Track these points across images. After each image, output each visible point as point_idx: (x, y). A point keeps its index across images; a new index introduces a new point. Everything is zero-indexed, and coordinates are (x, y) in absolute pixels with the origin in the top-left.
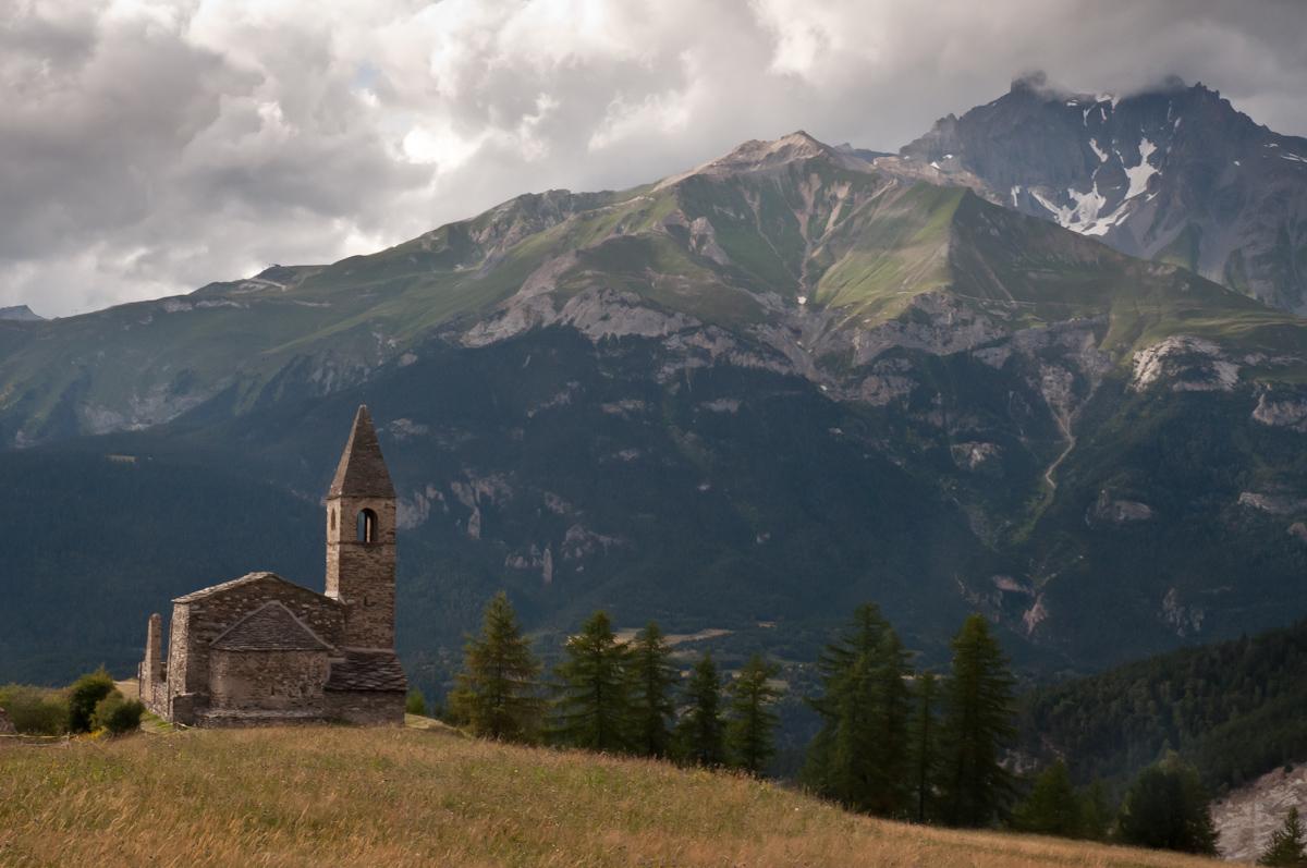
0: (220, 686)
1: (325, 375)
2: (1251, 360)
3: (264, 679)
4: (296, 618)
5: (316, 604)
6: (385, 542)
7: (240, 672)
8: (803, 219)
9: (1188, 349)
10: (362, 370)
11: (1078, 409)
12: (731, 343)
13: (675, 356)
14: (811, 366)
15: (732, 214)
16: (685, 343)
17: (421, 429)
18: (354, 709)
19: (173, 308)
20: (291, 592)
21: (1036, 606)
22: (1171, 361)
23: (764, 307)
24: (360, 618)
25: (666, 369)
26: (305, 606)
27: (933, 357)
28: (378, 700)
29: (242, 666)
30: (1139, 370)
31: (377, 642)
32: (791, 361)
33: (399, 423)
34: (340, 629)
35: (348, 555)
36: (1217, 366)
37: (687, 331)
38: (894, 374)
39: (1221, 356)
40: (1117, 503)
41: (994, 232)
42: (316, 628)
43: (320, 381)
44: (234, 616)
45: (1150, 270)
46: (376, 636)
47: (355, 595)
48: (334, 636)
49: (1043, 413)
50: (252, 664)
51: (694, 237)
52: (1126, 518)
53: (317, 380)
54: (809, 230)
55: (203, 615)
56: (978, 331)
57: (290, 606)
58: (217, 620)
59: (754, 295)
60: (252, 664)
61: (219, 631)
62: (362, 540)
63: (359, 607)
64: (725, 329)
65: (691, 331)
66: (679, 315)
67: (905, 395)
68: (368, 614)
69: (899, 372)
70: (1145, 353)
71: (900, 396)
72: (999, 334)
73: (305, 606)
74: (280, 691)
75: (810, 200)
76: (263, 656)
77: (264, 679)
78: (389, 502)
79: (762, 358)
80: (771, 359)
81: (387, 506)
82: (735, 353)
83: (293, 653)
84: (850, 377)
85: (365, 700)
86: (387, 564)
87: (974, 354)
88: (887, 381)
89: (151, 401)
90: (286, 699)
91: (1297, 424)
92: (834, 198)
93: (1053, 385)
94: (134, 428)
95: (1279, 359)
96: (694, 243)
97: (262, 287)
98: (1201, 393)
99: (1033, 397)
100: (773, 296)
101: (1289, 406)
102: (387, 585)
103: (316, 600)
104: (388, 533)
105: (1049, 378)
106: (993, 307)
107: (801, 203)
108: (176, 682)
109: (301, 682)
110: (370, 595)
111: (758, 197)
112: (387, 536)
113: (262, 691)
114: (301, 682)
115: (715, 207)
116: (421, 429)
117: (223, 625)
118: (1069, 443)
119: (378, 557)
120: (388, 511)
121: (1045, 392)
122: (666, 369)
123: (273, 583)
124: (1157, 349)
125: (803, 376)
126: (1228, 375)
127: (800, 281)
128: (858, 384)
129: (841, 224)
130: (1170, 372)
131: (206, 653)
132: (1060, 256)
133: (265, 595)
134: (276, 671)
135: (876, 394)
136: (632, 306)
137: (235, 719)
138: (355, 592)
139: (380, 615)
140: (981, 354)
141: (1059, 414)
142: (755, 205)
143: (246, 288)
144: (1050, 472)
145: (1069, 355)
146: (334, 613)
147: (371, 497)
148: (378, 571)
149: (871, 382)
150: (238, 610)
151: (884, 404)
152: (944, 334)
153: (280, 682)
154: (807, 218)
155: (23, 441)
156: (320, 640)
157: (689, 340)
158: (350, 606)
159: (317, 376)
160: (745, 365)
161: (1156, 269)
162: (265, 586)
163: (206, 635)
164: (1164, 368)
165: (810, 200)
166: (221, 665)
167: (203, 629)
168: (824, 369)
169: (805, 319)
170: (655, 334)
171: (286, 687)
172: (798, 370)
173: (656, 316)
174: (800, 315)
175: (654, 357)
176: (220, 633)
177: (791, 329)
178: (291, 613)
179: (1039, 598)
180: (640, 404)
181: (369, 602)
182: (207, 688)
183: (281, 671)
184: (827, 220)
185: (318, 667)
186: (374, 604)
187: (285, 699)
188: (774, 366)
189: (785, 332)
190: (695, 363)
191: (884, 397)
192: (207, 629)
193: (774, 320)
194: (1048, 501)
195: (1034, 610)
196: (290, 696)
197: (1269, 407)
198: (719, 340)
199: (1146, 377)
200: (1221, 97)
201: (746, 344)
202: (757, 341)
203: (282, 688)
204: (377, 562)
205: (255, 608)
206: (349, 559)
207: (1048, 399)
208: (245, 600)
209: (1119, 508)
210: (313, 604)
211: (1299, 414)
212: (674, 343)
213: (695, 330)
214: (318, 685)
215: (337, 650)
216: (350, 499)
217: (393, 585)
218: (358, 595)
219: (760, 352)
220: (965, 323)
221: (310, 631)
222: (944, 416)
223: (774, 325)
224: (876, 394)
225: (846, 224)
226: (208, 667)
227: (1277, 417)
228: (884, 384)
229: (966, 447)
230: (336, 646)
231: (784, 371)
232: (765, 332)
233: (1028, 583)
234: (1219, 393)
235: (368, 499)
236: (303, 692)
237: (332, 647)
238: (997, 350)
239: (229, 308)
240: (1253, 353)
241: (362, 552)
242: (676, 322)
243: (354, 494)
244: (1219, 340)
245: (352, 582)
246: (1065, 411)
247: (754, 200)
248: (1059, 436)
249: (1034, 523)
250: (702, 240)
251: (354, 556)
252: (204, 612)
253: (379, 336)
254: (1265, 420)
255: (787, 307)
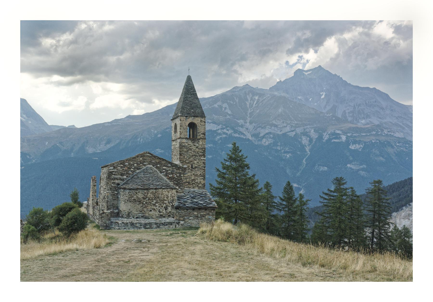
0: (123, 207)
1: (140, 139)
2: (349, 135)
3: (146, 203)
4: (159, 173)
5: (170, 167)
6: (201, 138)
7: (134, 199)
8: (248, 104)
9: (334, 132)
10: (149, 138)
11: (310, 146)
12: (233, 131)
13: (220, 134)
14: (250, 136)
15: (232, 103)
16: (222, 131)
17: (162, 151)
18: (190, 218)
19: (106, 125)
20: (157, 161)
21: (302, 190)
22: (331, 135)
23: (239, 123)
24: (189, 174)
25: (218, 137)
26: (164, 168)
27: (278, 134)
28: (202, 214)
29: (135, 196)
30: (324, 137)
31: (198, 186)
32: (246, 135)
33: (157, 150)
34: (181, 179)
35: (183, 144)
36: (341, 136)
37: (222, 129)
38: (269, 138)
39: (342, 134)
40: (319, 167)
41: (291, 106)
42: (169, 178)
43: (140, 141)
44: (130, 172)
45: (326, 115)
46: (197, 183)
47: (187, 163)
48: (178, 182)
49: (303, 147)
50: (140, 195)
51: (224, 108)
52: (322, 170)
53: (139, 141)
54: (249, 106)
55: (116, 172)
56: (288, 129)
57: (157, 168)
58: (122, 175)
59: (237, 121)
60: (140, 195)
61: (123, 180)
62: (188, 137)
63: (189, 169)
64: (231, 128)
65: (223, 129)
66: (221, 125)
67: (272, 143)
68: (193, 172)
69: (270, 138)
70: (325, 133)
71: (270, 143)
72: (293, 129)
73: (164, 168)
74: (154, 209)
75: (249, 99)
76: (145, 191)
77: (146, 203)
78: (203, 120)
79: (239, 135)
80: (241, 135)
81: (201, 121)
82: (233, 134)
83: (160, 190)
84: (259, 139)
85: (196, 213)
86: (202, 148)
87: (287, 133)
88: (267, 140)
89: (101, 146)
90: (157, 213)
91: (359, 149)
92: (255, 99)
93: (305, 141)
94: (98, 152)
95: (355, 134)
96: (224, 109)
97: (126, 120)
98: (338, 142)
99: (300, 143)
100: (242, 121)
101: (357, 145)
102: (202, 158)
103: (170, 165)
104: (202, 134)
105: (304, 139)
106: (291, 123)
107: (247, 100)
108: (102, 205)
109: (165, 205)
110: (194, 163)
111: (238, 99)
112: (202, 135)
113: (145, 209)
114: (165, 205)
115: (228, 101)
116: (162, 151)
117: (125, 177)
118: (308, 153)
119: (197, 145)
120: (202, 123)
121: (303, 142)
122: (218, 137)
123: (148, 156)
124: (328, 132)
125: (249, 138)
126: (344, 138)
127: (248, 117)
128: (261, 140)
129: (257, 105)
130: (331, 137)
131: (116, 191)
132: (305, 112)
133: (145, 162)
134: (152, 199)
135: (265, 143)
136: (210, 123)
137: (132, 224)
138: (187, 161)
139: (199, 173)
140: (289, 134)
141: (306, 147)
142: (237, 101)
143: (123, 120)
144: (304, 160)
145: (308, 134)
146: (178, 171)
147: (194, 116)
148: (198, 152)
149: (264, 140)
150: (132, 169)
151: (267, 145)
152: (280, 129)
153: (154, 205)
154: (249, 103)
155: (73, 155)
156: (171, 184)
157: (223, 130)
158: (185, 168)
159: (139, 139)
160: (236, 136)
161: (327, 115)
162: (145, 158)
163: (117, 181)
164: (330, 136)
165: (249, 99)
166: (123, 196)
167: (115, 179)
168: (253, 137)
169: (249, 126)
170: (215, 129)
171: (157, 207)
172: (247, 137)
173: (216, 126)
174: (248, 125)
175: (215, 135)
176: (123, 181)
177: (246, 128)
178: (158, 171)
179: (303, 188)
180: (212, 145)
181: (194, 166)
182: (117, 208)
183: (155, 199)
184: (253, 103)
185: (173, 197)
186: (196, 167)
187: (157, 214)
188: (242, 136)
189: (244, 129)
190: (224, 136)
191: (267, 143)
192: (117, 179)
193: (242, 126)
194: (304, 167)
195: (302, 191)
196: (160, 212)
197: (353, 145)
198: (230, 131)
199: (326, 139)
200: (340, 77)
201: (236, 132)
202: (238, 131)
203: (155, 208)
204: (197, 147)
205: (140, 169)
206: (184, 146)
207: (304, 144)
208: (135, 165)
209: (320, 168)
210: (168, 167)
211: (360, 147)
212: (219, 131)
213: (224, 128)
214: (172, 206)
215: (180, 189)
216: (185, 117)
217: (205, 159)
218: (189, 163)
219: (239, 133)
220: (285, 127)
221: (167, 180)
222: (280, 148)
223: (242, 127)
224: (265, 143)
225: (258, 105)
226: (118, 198)
227: (355, 147)
228: (267, 140)
229: (285, 155)
230: (179, 187)
231: (245, 137)
232: (240, 129)
233: (300, 185)
234: (342, 142)
235: (193, 118)
236: (166, 210)
237: (177, 188)
238: (292, 133)
239: (119, 124)
240: (349, 133)
241: (190, 142)
242: (220, 127)
243: (186, 115)
244: (341, 130)
245: (186, 157)
246: (308, 146)
247: (237, 99)
248: (306, 152)
249: (301, 171)
250: (225, 108)
251: (187, 144)
252: (116, 170)
253: (153, 130)
254: (352, 148)
255: (245, 123)
